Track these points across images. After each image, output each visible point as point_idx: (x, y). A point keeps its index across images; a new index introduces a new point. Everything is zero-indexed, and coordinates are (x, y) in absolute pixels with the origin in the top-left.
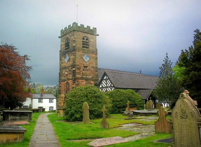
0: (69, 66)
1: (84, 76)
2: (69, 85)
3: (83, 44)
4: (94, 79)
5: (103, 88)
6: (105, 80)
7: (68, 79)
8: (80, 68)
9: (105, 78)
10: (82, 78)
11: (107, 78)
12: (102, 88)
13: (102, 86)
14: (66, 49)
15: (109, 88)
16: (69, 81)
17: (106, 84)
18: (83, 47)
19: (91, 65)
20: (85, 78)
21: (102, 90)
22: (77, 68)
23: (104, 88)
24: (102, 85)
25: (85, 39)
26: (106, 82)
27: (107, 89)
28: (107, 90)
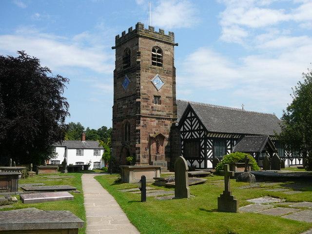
0: (130, 96)
1: (154, 113)
2: (129, 128)
3: (153, 59)
4: (171, 117)
6: (189, 118)
7: (127, 116)
8: (148, 99)
9: (189, 116)
10: (151, 116)
11: (193, 115)
12: (183, 132)
13: (184, 128)
14: (125, 67)
15: (196, 132)
16: (129, 121)
17: (191, 126)
18: (154, 64)
19: (166, 95)
20: (157, 115)
21: (184, 135)
22: (143, 99)
23: (196, 131)
24: (184, 127)
25: (157, 50)
27: (198, 136)
28: (192, 136)
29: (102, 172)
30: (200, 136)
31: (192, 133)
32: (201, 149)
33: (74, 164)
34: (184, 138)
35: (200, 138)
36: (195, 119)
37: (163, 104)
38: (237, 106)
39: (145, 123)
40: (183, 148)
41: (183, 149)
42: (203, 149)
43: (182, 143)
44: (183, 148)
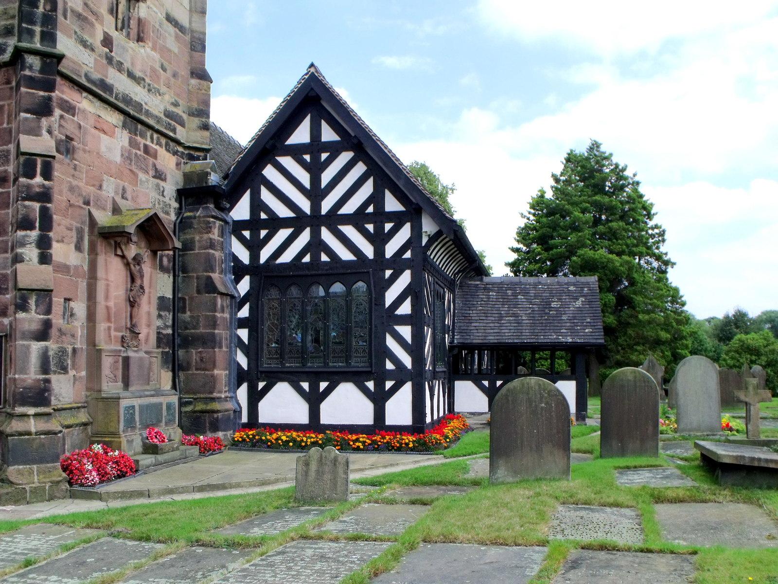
5: (275, 223)
6: (296, 152)
9: (301, 135)
11: (328, 134)
12: (253, 224)
13: (257, 205)
15: (349, 231)
17: (316, 194)
21: (254, 246)
26: (315, 169)
27: (368, 250)
28: (316, 245)
30: (379, 251)
32: (391, 318)
34: (254, 256)
36: (345, 157)
37: (154, 48)
40: (244, 312)
41: (242, 323)
42: (404, 320)
43: (244, 286)
44: (244, 312)
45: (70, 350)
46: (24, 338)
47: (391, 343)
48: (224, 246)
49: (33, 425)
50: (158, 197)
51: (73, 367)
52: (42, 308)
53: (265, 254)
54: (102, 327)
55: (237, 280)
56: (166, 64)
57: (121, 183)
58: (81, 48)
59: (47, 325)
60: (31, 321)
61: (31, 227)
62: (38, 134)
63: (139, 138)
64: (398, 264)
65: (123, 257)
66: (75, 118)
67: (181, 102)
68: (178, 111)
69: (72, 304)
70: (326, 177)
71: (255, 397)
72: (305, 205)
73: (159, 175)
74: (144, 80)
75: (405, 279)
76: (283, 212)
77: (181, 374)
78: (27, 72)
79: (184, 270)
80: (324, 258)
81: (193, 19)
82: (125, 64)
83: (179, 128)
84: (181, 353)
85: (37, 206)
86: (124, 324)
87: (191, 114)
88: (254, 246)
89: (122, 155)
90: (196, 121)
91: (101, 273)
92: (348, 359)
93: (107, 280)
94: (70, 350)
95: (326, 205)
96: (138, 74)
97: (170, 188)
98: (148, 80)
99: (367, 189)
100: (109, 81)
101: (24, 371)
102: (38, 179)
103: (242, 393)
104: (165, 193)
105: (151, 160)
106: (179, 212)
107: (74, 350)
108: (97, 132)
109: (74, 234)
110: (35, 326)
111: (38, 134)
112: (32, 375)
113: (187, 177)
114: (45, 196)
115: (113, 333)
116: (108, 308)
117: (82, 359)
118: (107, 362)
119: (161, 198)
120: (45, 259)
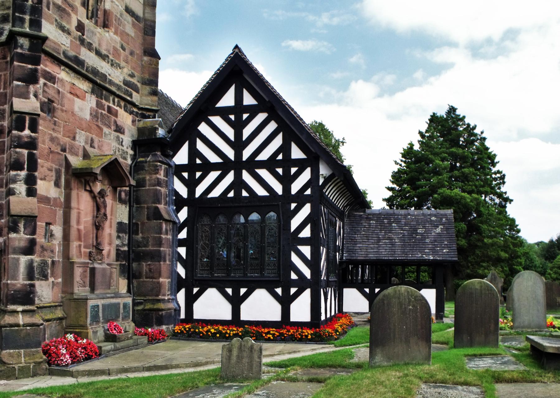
5: (207, 167)
6: (224, 113)
11: (248, 100)
12: (191, 167)
13: (194, 153)
15: (264, 173)
21: (191, 185)
23: (263, 164)
26: (239, 126)
27: (278, 188)
28: (239, 184)
29: (323, 348)
31: (238, 176)
33: (550, 143)
34: (191, 192)
35: (287, 195)
36: (261, 117)
37: (116, 33)
38: (205, 134)
39: (52, 93)
40: (183, 235)
41: (181, 243)
42: (304, 242)
43: (183, 215)
44: (183, 235)
45: (50, 261)
46: (15, 252)
47: (295, 259)
48: (169, 184)
49: (21, 319)
50: (118, 146)
51: (52, 275)
52: (29, 230)
53: (199, 190)
54: (74, 244)
55: (178, 210)
56: (125, 45)
57: (90, 135)
58: (60, 32)
59: (33, 243)
60: (20, 240)
61: (22, 169)
62: (27, 97)
63: (104, 101)
64: (301, 199)
65: (91, 192)
66: (56, 86)
67: (136, 74)
68: (134, 81)
69: (52, 227)
70: (247, 132)
71: (191, 300)
72: (230, 153)
73: (119, 130)
74: (108, 57)
75: (306, 210)
76: (213, 158)
77: (135, 282)
78: (19, 50)
79: (138, 201)
80: (245, 194)
81: (146, 11)
82: (94, 45)
83: (134, 94)
84: (134, 265)
85: (25, 152)
86: (91, 242)
87: (144, 83)
88: (191, 185)
89: (91, 114)
90: (148, 89)
91: (74, 204)
92: (262, 270)
93: (78, 209)
94: (50, 261)
95: (247, 153)
96: (104, 52)
97: (127, 139)
98: (111, 57)
99: (278, 142)
100: (82, 57)
101: (15, 277)
102: (27, 132)
103: (181, 296)
104: (124, 143)
105: (113, 118)
106: (134, 158)
107: (53, 262)
108: (72, 96)
109: (54, 174)
110: (23, 244)
111: (27, 97)
112: (21, 281)
113: (140, 131)
114: (31, 145)
115: (83, 250)
116: (79, 230)
117: (59, 269)
118: (78, 272)
119: (121, 147)
120: (31, 192)
